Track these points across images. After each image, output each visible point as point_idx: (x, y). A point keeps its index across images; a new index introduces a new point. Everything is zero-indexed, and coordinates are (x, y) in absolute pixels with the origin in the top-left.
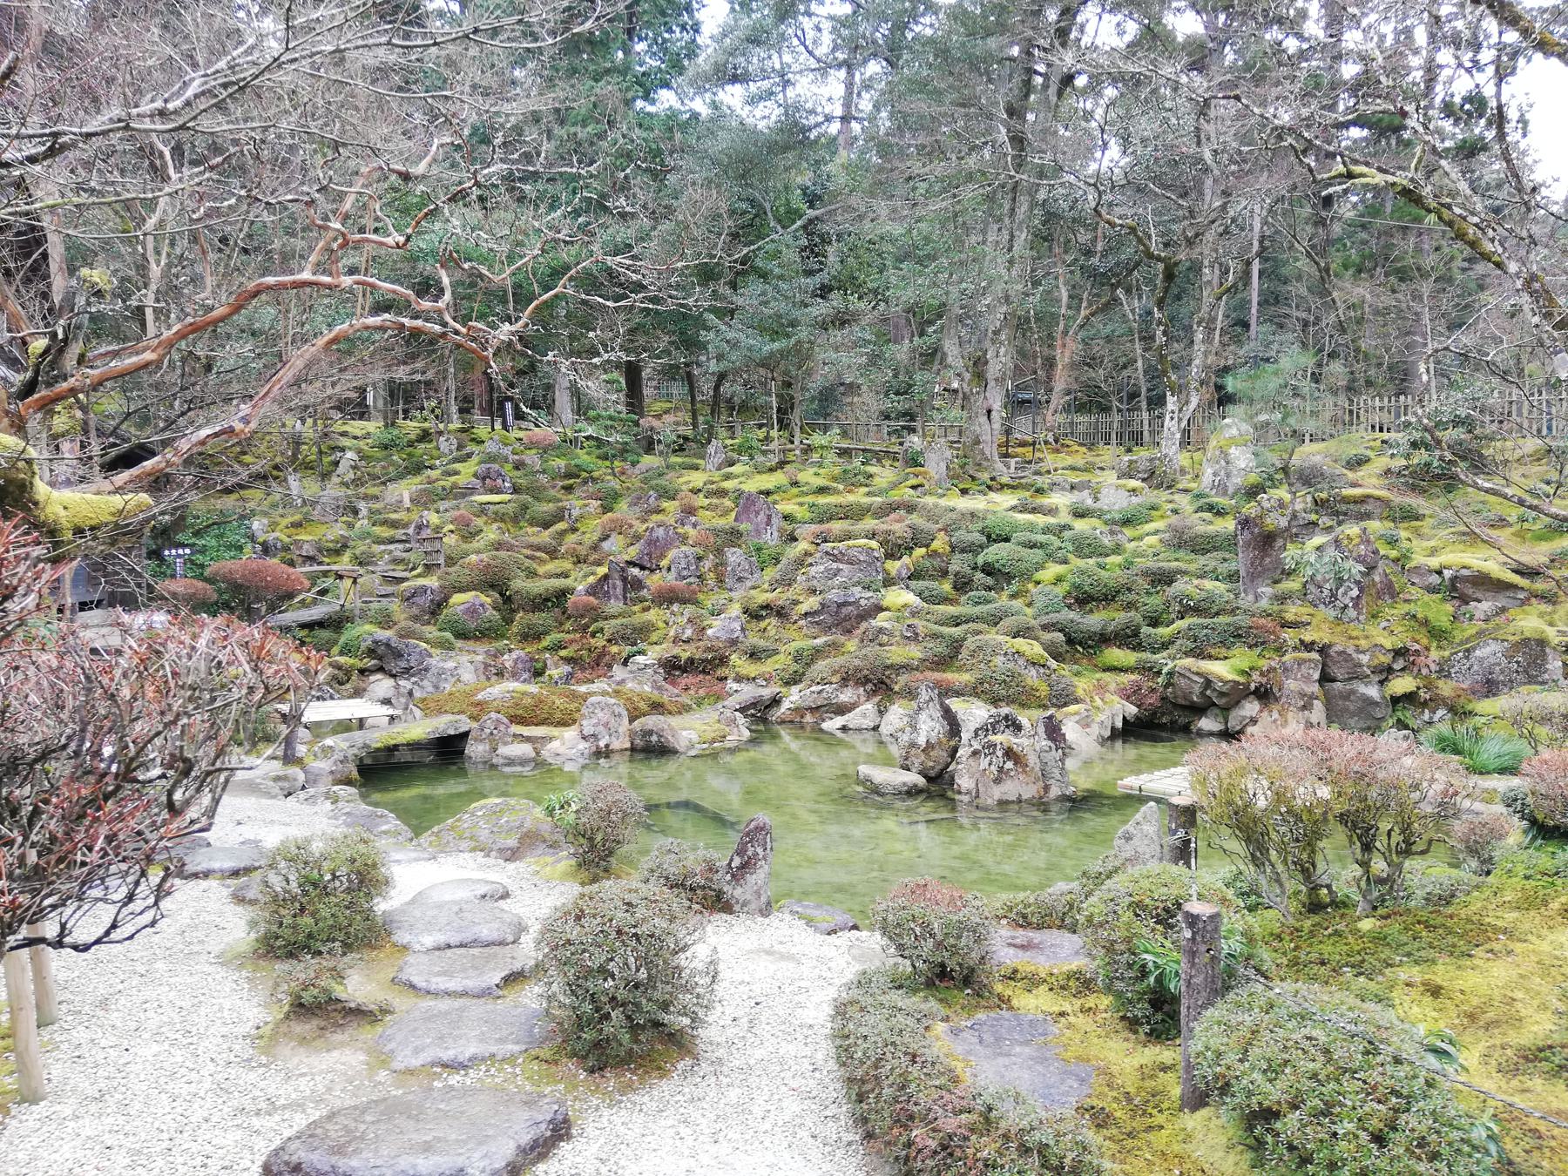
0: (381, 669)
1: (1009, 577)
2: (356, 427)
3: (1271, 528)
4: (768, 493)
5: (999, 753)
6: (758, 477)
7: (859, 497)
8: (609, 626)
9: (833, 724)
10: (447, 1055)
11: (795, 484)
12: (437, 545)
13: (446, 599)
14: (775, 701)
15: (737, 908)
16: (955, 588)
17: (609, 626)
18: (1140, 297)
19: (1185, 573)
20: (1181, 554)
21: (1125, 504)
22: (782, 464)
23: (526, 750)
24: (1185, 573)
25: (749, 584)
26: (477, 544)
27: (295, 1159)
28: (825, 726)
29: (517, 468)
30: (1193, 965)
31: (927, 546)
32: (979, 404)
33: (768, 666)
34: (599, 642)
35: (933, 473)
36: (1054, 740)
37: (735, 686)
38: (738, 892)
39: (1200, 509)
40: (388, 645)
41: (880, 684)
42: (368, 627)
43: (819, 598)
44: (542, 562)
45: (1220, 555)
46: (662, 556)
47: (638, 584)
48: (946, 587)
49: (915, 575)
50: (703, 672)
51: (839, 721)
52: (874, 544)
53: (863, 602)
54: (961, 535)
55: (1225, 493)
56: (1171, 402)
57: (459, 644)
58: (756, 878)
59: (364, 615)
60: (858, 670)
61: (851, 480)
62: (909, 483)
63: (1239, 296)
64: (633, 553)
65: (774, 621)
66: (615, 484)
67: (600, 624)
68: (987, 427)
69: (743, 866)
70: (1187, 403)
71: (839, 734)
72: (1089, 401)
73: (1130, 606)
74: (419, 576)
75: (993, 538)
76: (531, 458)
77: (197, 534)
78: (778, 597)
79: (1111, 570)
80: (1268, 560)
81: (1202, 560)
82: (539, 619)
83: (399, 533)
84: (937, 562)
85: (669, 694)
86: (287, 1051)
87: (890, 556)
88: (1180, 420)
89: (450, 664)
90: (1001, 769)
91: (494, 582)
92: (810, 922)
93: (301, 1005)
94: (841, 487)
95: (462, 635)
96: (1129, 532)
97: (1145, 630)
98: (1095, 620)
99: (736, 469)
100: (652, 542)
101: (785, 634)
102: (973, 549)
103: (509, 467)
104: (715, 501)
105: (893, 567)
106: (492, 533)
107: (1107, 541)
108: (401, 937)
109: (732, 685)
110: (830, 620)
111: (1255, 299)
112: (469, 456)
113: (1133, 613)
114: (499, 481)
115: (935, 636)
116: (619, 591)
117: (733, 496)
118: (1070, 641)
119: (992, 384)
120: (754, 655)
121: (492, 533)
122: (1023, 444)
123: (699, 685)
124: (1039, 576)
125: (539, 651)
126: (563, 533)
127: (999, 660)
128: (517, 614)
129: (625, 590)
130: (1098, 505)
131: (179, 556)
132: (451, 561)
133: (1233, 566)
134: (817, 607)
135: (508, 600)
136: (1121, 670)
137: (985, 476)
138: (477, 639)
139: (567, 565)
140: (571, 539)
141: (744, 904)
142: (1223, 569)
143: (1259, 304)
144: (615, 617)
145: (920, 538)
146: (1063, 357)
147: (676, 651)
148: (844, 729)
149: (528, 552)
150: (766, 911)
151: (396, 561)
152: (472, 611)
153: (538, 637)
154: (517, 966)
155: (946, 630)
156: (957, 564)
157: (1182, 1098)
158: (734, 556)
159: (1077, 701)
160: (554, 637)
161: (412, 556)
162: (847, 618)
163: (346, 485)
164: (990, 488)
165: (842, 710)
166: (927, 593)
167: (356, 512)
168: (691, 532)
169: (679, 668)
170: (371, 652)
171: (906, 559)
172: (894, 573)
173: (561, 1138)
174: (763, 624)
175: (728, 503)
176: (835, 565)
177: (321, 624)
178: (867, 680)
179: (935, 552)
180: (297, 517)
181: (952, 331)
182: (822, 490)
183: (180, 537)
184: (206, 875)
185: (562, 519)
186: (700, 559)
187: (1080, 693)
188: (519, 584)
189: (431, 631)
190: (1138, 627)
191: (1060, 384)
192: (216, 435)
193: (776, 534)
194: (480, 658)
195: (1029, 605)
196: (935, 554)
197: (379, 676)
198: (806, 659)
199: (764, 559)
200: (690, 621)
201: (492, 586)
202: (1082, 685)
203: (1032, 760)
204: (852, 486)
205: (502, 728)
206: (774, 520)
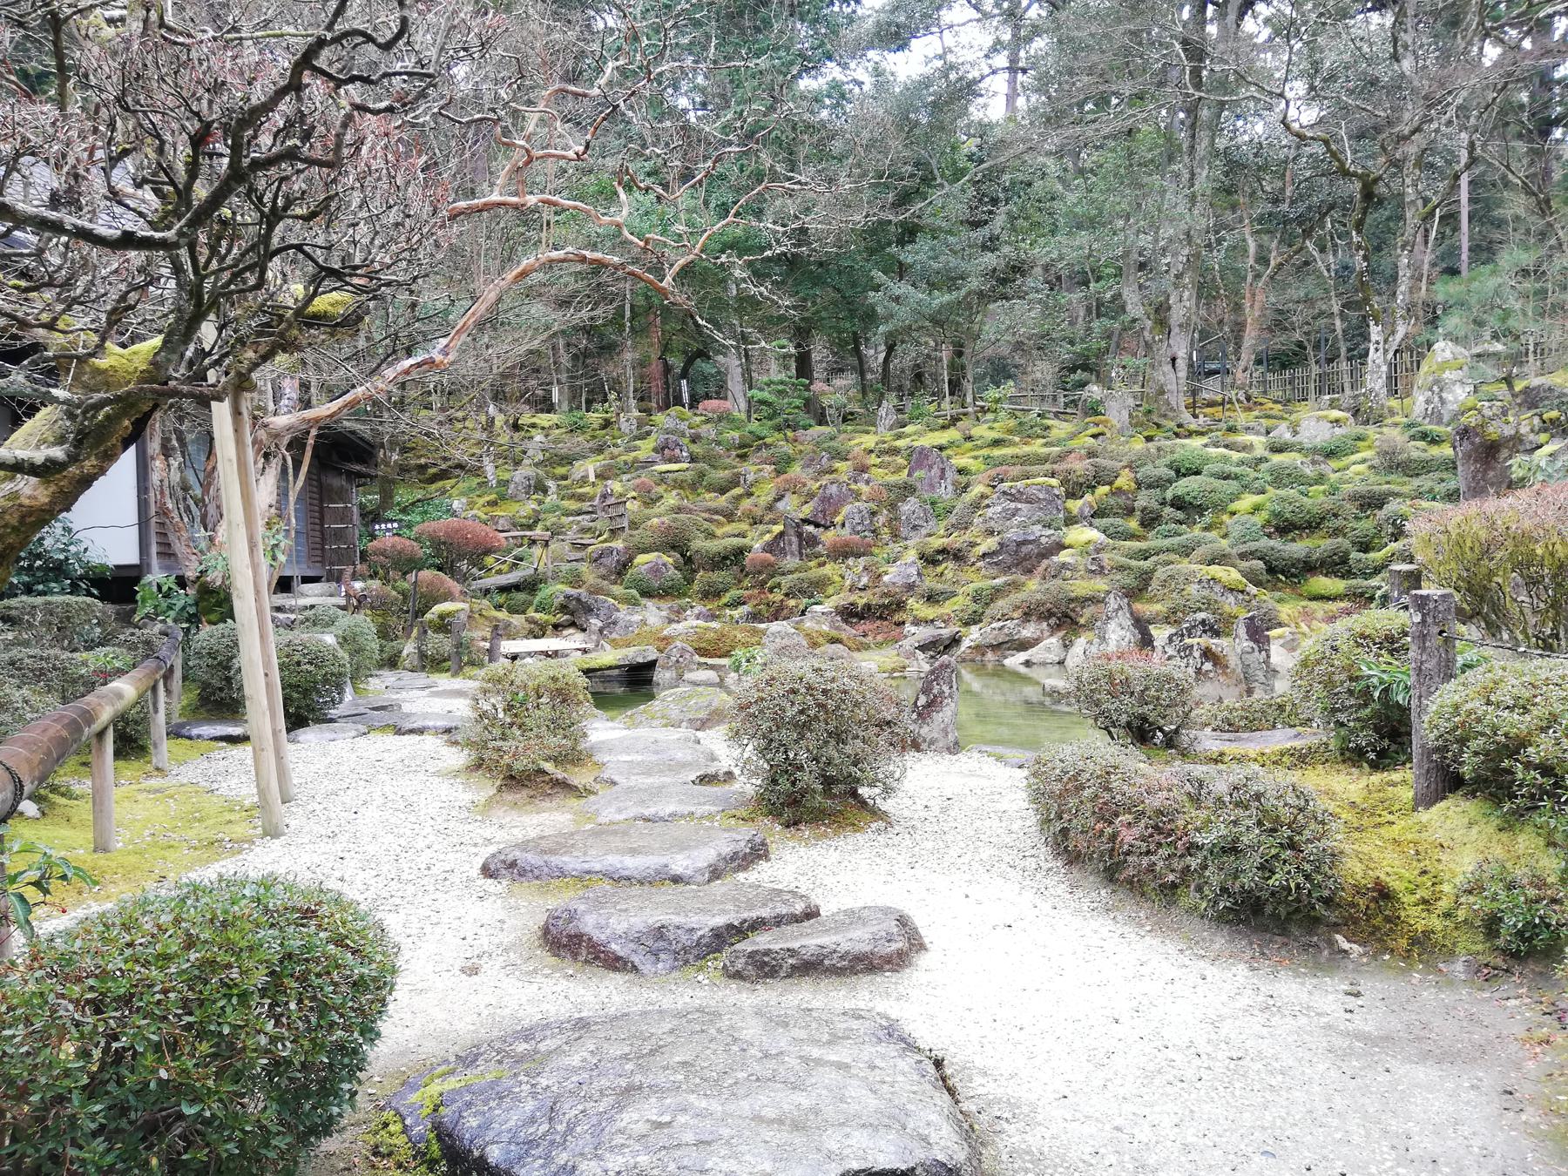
0: (573, 624)
1: (1201, 510)
2: (544, 419)
3: (1494, 437)
4: (941, 448)
5: (1197, 654)
6: (931, 434)
7: (1037, 447)
8: (786, 582)
9: (1015, 661)
10: (647, 813)
11: (969, 438)
12: (621, 510)
13: (631, 559)
14: (955, 641)
15: (924, 746)
16: (1142, 524)
17: (786, 582)
18: (1335, 253)
19: (1397, 495)
20: (1392, 477)
21: (1327, 436)
22: (954, 420)
23: (711, 675)
24: (1397, 495)
25: (924, 531)
26: (660, 508)
27: (510, 858)
28: (1007, 662)
29: (694, 442)
30: (1423, 649)
31: (1111, 484)
32: (1163, 352)
33: (947, 608)
34: (777, 596)
35: (1115, 422)
36: (1256, 641)
37: (913, 629)
38: (925, 730)
39: (1413, 438)
40: (578, 600)
41: (1065, 618)
42: (560, 587)
43: (997, 539)
44: (719, 524)
45: (1437, 475)
46: (836, 513)
47: (813, 541)
48: (1133, 524)
49: (1099, 513)
50: (880, 618)
51: (1022, 656)
52: (1054, 482)
53: (1044, 540)
54: (1148, 471)
55: (1440, 422)
56: (1375, 332)
57: (644, 601)
58: (944, 715)
59: (556, 576)
60: (1040, 604)
61: (1026, 432)
62: (1090, 432)
63: (1447, 242)
64: (807, 511)
65: (950, 565)
66: (788, 449)
67: (777, 579)
68: (1172, 375)
69: (929, 705)
70: (1393, 333)
71: (1023, 670)
72: (1282, 361)
73: (1337, 532)
74: (605, 541)
75: (1182, 471)
76: (708, 431)
77: (404, 511)
78: (957, 540)
79: (1316, 499)
80: (1491, 474)
81: (1416, 482)
82: (717, 577)
83: (586, 506)
84: (1121, 500)
85: (847, 632)
86: (500, 813)
87: (1071, 495)
88: (1386, 351)
89: (637, 618)
90: (1198, 671)
91: (675, 543)
92: (999, 758)
93: (512, 777)
94: (1017, 439)
95: (647, 593)
96: (1334, 464)
97: (1354, 555)
98: (1298, 548)
99: (909, 429)
100: (826, 500)
101: (963, 577)
102: (1159, 484)
103: (686, 441)
104: (887, 458)
105: (1075, 506)
106: (671, 499)
107: (1309, 471)
108: (598, 758)
109: (909, 628)
110: (1009, 560)
111: (1465, 245)
112: (648, 433)
113: (1340, 539)
114: (677, 451)
115: (1121, 568)
116: (795, 547)
117: (905, 453)
118: (1271, 570)
119: (1176, 330)
120: (931, 598)
121: (671, 499)
122: (1212, 404)
123: (878, 631)
124: (1233, 507)
125: (720, 608)
126: (739, 498)
127: (1193, 589)
128: (698, 572)
129: (800, 545)
130: (1297, 439)
131: (388, 530)
132: (634, 525)
133: (1452, 485)
134: (995, 547)
135: (689, 561)
136: (1328, 599)
137: (1172, 424)
138: (661, 597)
139: (744, 526)
140: (746, 504)
141: (932, 742)
142: (1441, 488)
143: (1470, 250)
144: (791, 572)
145: (1100, 478)
146: (1251, 314)
147: (853, 598)
148: (1028, 664)
149: (706, 515)
150: (955, 748)
151: (584, 530)
152: (656, 570)
153: (718, 594)
154: (711, 770)
155: (1134, 563)
156: (1144, 500)
157: (1415, 799)
158: (909, 507)
159: (1280, 625)
160: (734, 593)
161: (598, 525)
162: (1027, 557)
163: (536, 465)
164: (1177, 435)
165: (1023, 646)
166: (1112, 530)
167: (545, 491)
168: (865, 489)
169: (856, 615)
170: (563, 608)
171: (1088, 497)
172: (1075, 511)
173: (760, 857)
174: (939, 569)
175: (900, 460)
176: (1013, 505)
177: (517, 587)
178: (1051, 614)
179: (1119, 489)
180: (493, 497)
181: (1131, 278)
182: (997, 443)
183: (389, 514)
184: (420, 731)
185: (737, 484)
186: (874, 514)
187: (1283, 617)
188: (699, 544)
189: (617, 589)
190: (1347, 553)
191: (1250, 338)
192: (419, 365)
193: (950, 488)
194: (664, 613)
195: (1225, 536)
196: (1120, 491)
197: (571, 631)
198: (985, 599)
199: (937, 510)
200: (865, 568)
201: (673, 548)
202: (1286, 611)
203: (1233, 661)
204: (1029, 437)
205: (687, 656)
206: (948, 474)
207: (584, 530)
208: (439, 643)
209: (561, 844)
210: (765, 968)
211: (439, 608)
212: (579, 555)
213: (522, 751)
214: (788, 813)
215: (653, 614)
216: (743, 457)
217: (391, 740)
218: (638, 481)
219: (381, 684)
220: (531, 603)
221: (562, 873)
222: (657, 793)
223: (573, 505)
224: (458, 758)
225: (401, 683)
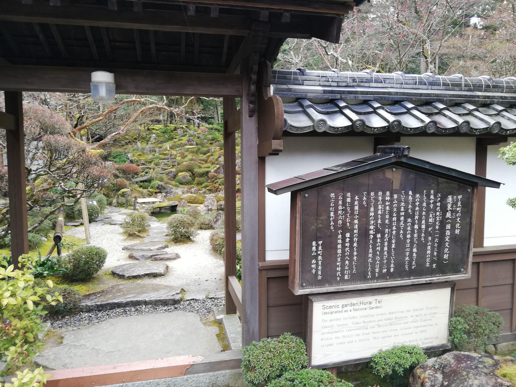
12: (175, 160)
13: (177, 174)
26: (186, 159)
34: (217, 185)
40: (162, 186)
42: (157, 182)
44: (203, 164)
69: (216, 221)
77: (114, 158)
82: (201, 179)
95: (181, 184)
106: (190, 157)
112: (186, 135)
121: (190, 157)
126: (209, 156)
135: (193, 174)
138: (185, 184)
139: (209, 165)
140: (211, 157)
149: (199, 161)
151: (165, 164)
152: (184, 177)
153: (201, 184)
161: (169, 163)
170: (158, 188)
177: (145, 181)
183: (110, 159)
184: (115, 224)
185: (209, 152)
188: (197, 170)
189: (173, 183)
192: (116, 134)
201: (189, 171)
207: (165, 164)
208: (122, 200)
209: (135, 245)
210: (156, 260)
211: (122, 190)
212: (163, 172)
213: (135, 230)
214: (175, 241)
215: (179, 191)
216: (211, 144)
217: (109, 226)
218: (180, 151)
219: (107, 211)
220: (149, 186)
221: (134, 249)
222: (156, 237)
223: (162, 157)
224: (121, 230)
225: (112, 211)
